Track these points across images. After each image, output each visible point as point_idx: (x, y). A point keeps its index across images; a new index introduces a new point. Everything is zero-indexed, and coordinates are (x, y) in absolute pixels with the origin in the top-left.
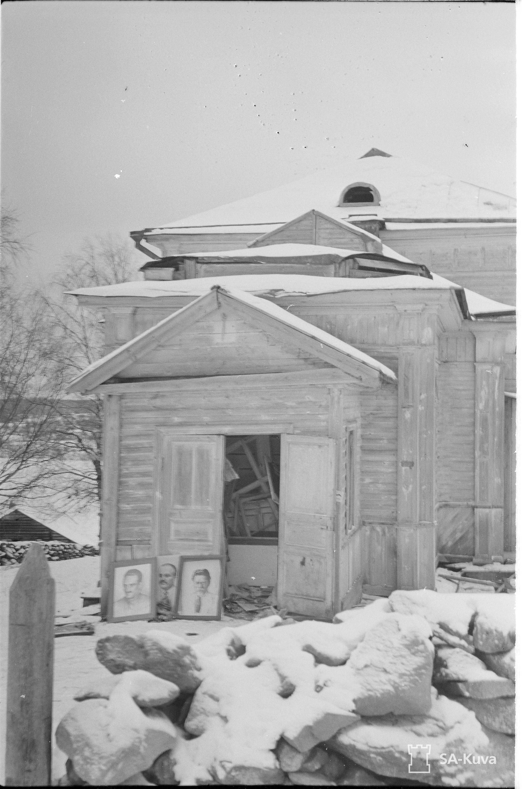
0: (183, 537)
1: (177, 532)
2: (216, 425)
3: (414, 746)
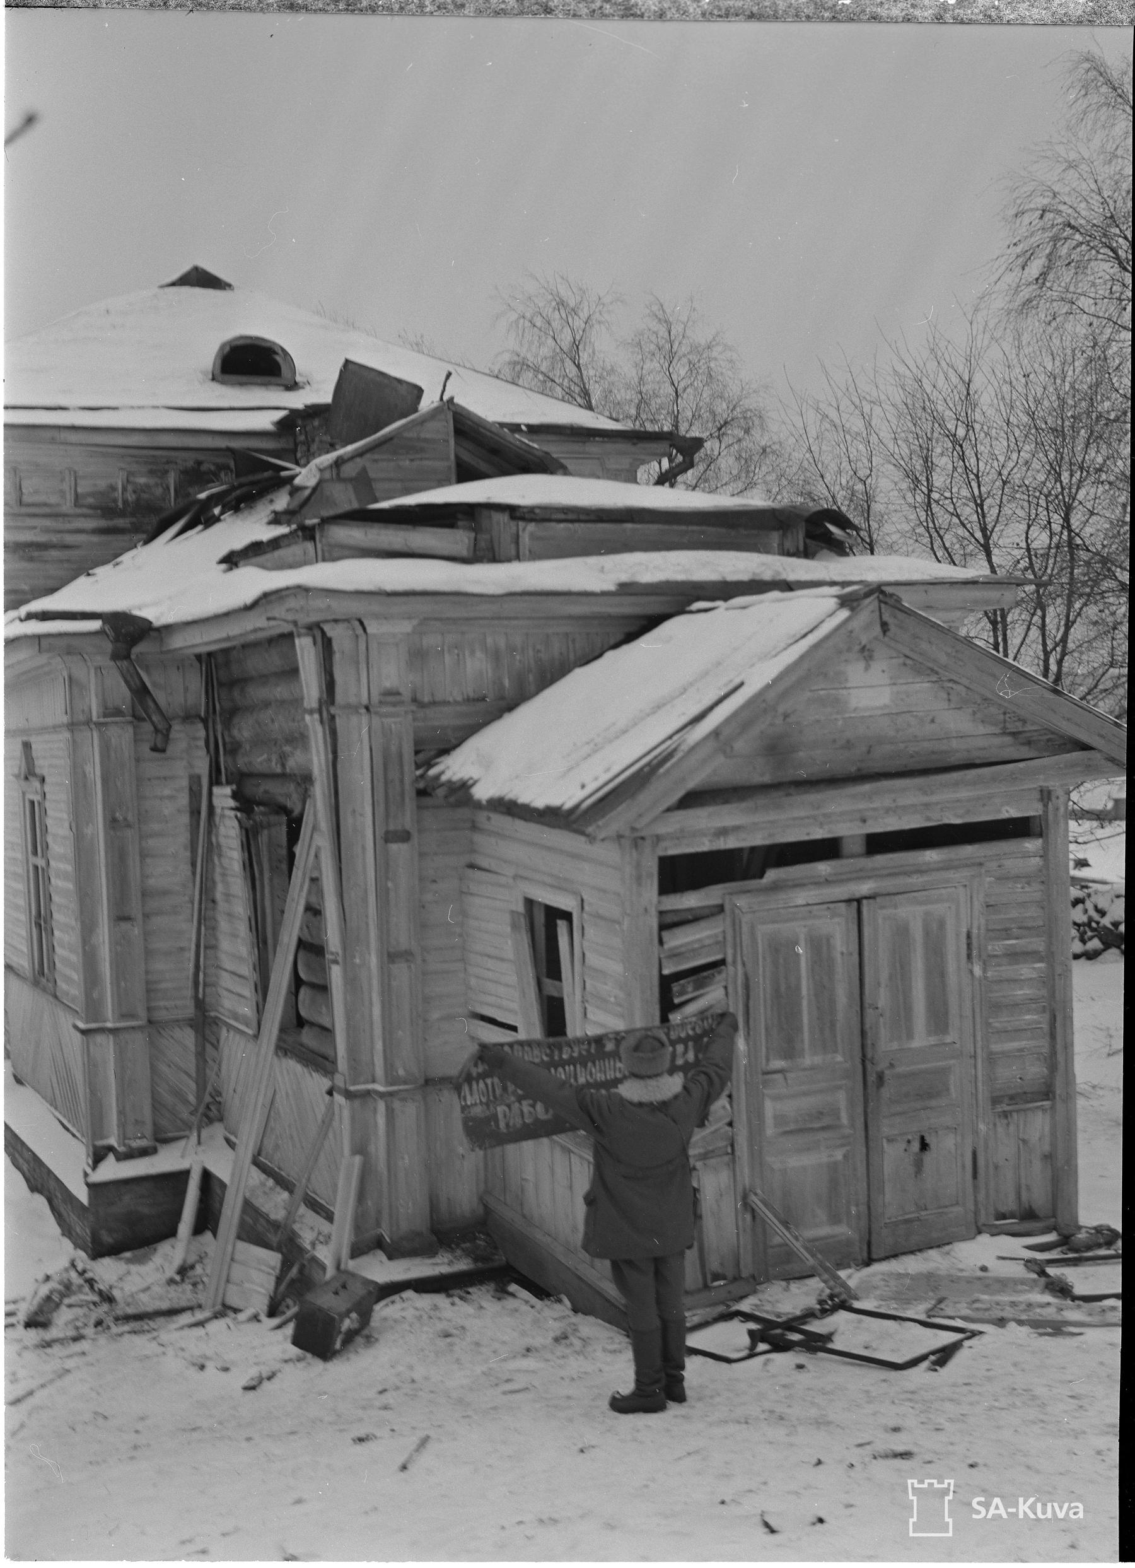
0: (792, 1127)
1: (780, 1119)
2: (842, 881)
3: (921, 1482)
